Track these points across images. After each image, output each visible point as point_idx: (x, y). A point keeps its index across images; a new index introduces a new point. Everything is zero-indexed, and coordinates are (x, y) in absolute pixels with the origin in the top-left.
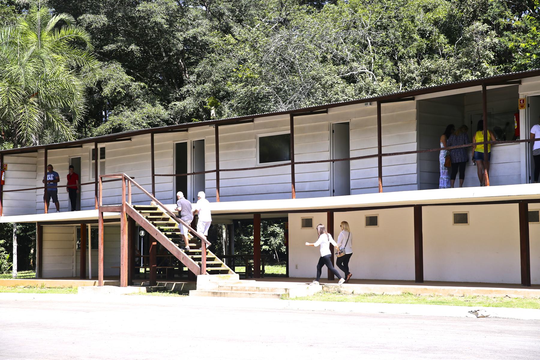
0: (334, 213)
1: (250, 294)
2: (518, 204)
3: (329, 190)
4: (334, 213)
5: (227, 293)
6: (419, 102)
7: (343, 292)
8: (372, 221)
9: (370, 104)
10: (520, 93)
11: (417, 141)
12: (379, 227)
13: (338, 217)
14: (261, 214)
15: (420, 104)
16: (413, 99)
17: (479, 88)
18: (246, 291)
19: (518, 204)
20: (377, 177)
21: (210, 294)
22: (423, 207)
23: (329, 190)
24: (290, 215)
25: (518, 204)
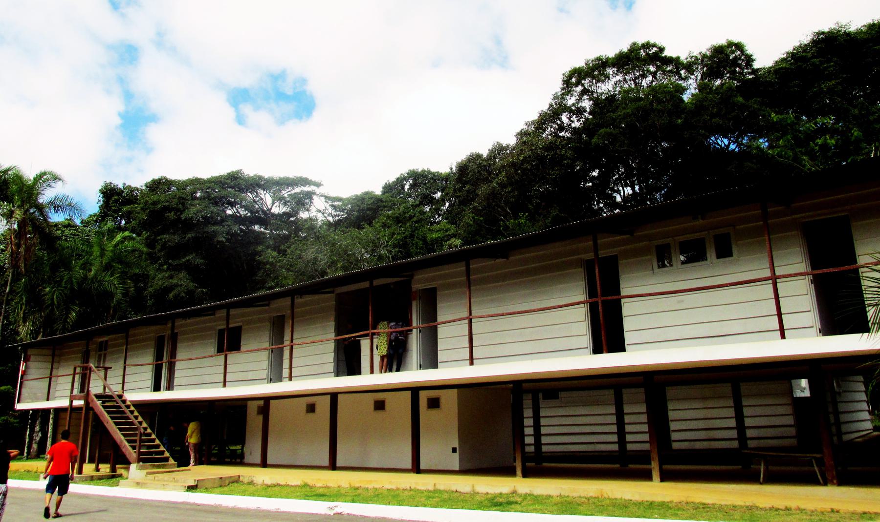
0: (271, 401)
1: (164, 485)
2: (410, 391)
3: (266, 379)
4: (271, 401)
5: (147, 483)
6: (338, 294)
7: (246, 480)
8: (380, 406)
9: (301, 298)
10: (413, 286)
11: (335, 332)
12: (386, 411)
13: (424, 396)
14: (524, 384)
15: (340, 298)
16: (332, 292)
17: (365, 285)
18: (165, 481)
19: (612, 392)
20: (786, 329)
21: (135, 484)
22: (339, 396)
23: (266, 379)
24: (249, 403)
25: (410, 391)
